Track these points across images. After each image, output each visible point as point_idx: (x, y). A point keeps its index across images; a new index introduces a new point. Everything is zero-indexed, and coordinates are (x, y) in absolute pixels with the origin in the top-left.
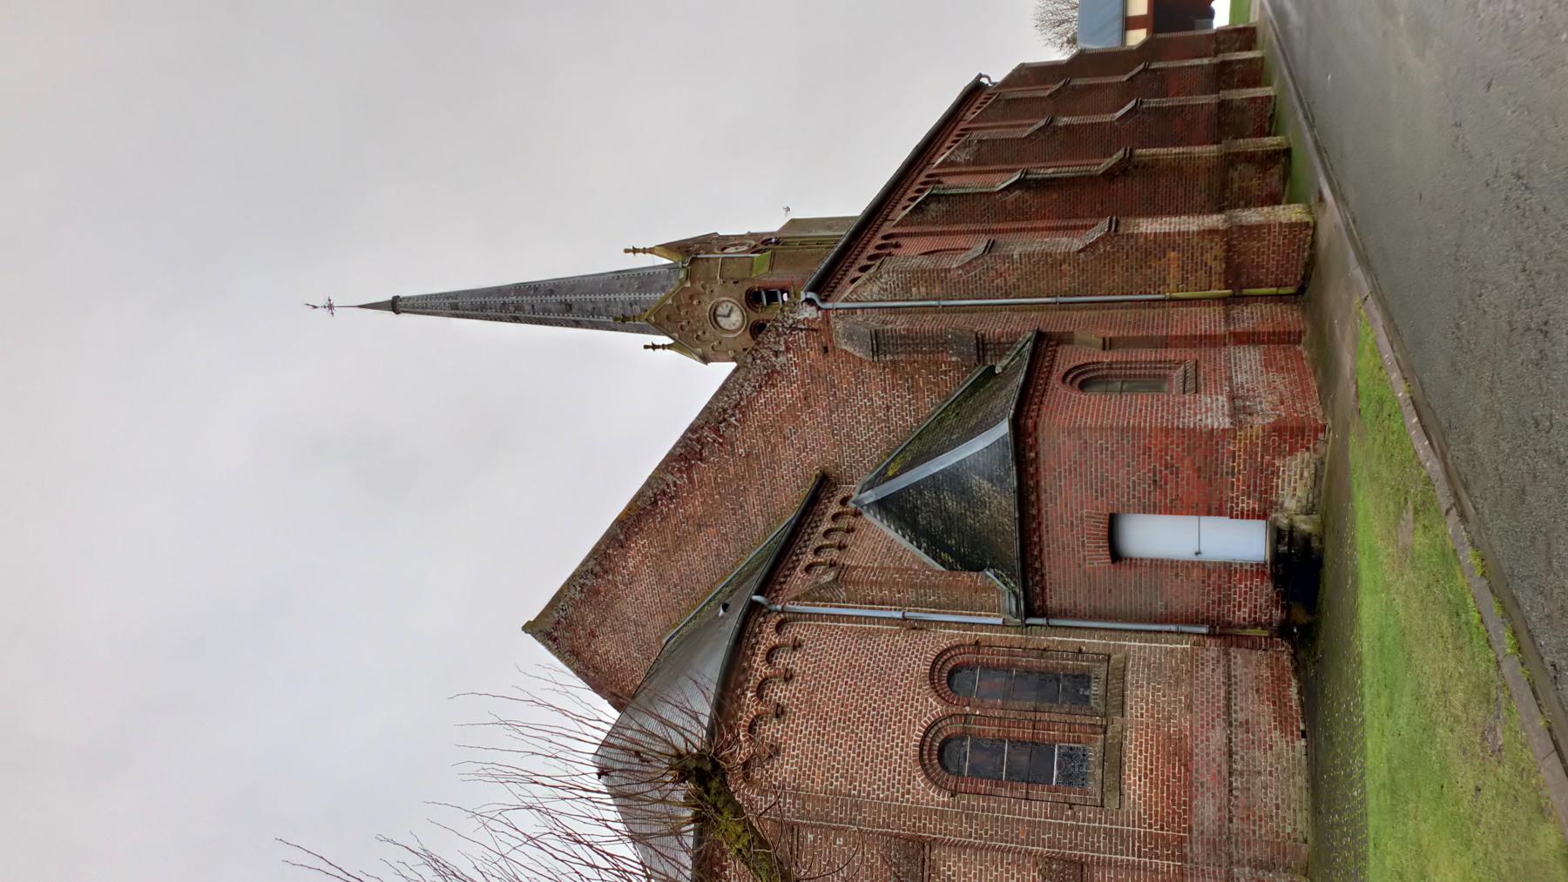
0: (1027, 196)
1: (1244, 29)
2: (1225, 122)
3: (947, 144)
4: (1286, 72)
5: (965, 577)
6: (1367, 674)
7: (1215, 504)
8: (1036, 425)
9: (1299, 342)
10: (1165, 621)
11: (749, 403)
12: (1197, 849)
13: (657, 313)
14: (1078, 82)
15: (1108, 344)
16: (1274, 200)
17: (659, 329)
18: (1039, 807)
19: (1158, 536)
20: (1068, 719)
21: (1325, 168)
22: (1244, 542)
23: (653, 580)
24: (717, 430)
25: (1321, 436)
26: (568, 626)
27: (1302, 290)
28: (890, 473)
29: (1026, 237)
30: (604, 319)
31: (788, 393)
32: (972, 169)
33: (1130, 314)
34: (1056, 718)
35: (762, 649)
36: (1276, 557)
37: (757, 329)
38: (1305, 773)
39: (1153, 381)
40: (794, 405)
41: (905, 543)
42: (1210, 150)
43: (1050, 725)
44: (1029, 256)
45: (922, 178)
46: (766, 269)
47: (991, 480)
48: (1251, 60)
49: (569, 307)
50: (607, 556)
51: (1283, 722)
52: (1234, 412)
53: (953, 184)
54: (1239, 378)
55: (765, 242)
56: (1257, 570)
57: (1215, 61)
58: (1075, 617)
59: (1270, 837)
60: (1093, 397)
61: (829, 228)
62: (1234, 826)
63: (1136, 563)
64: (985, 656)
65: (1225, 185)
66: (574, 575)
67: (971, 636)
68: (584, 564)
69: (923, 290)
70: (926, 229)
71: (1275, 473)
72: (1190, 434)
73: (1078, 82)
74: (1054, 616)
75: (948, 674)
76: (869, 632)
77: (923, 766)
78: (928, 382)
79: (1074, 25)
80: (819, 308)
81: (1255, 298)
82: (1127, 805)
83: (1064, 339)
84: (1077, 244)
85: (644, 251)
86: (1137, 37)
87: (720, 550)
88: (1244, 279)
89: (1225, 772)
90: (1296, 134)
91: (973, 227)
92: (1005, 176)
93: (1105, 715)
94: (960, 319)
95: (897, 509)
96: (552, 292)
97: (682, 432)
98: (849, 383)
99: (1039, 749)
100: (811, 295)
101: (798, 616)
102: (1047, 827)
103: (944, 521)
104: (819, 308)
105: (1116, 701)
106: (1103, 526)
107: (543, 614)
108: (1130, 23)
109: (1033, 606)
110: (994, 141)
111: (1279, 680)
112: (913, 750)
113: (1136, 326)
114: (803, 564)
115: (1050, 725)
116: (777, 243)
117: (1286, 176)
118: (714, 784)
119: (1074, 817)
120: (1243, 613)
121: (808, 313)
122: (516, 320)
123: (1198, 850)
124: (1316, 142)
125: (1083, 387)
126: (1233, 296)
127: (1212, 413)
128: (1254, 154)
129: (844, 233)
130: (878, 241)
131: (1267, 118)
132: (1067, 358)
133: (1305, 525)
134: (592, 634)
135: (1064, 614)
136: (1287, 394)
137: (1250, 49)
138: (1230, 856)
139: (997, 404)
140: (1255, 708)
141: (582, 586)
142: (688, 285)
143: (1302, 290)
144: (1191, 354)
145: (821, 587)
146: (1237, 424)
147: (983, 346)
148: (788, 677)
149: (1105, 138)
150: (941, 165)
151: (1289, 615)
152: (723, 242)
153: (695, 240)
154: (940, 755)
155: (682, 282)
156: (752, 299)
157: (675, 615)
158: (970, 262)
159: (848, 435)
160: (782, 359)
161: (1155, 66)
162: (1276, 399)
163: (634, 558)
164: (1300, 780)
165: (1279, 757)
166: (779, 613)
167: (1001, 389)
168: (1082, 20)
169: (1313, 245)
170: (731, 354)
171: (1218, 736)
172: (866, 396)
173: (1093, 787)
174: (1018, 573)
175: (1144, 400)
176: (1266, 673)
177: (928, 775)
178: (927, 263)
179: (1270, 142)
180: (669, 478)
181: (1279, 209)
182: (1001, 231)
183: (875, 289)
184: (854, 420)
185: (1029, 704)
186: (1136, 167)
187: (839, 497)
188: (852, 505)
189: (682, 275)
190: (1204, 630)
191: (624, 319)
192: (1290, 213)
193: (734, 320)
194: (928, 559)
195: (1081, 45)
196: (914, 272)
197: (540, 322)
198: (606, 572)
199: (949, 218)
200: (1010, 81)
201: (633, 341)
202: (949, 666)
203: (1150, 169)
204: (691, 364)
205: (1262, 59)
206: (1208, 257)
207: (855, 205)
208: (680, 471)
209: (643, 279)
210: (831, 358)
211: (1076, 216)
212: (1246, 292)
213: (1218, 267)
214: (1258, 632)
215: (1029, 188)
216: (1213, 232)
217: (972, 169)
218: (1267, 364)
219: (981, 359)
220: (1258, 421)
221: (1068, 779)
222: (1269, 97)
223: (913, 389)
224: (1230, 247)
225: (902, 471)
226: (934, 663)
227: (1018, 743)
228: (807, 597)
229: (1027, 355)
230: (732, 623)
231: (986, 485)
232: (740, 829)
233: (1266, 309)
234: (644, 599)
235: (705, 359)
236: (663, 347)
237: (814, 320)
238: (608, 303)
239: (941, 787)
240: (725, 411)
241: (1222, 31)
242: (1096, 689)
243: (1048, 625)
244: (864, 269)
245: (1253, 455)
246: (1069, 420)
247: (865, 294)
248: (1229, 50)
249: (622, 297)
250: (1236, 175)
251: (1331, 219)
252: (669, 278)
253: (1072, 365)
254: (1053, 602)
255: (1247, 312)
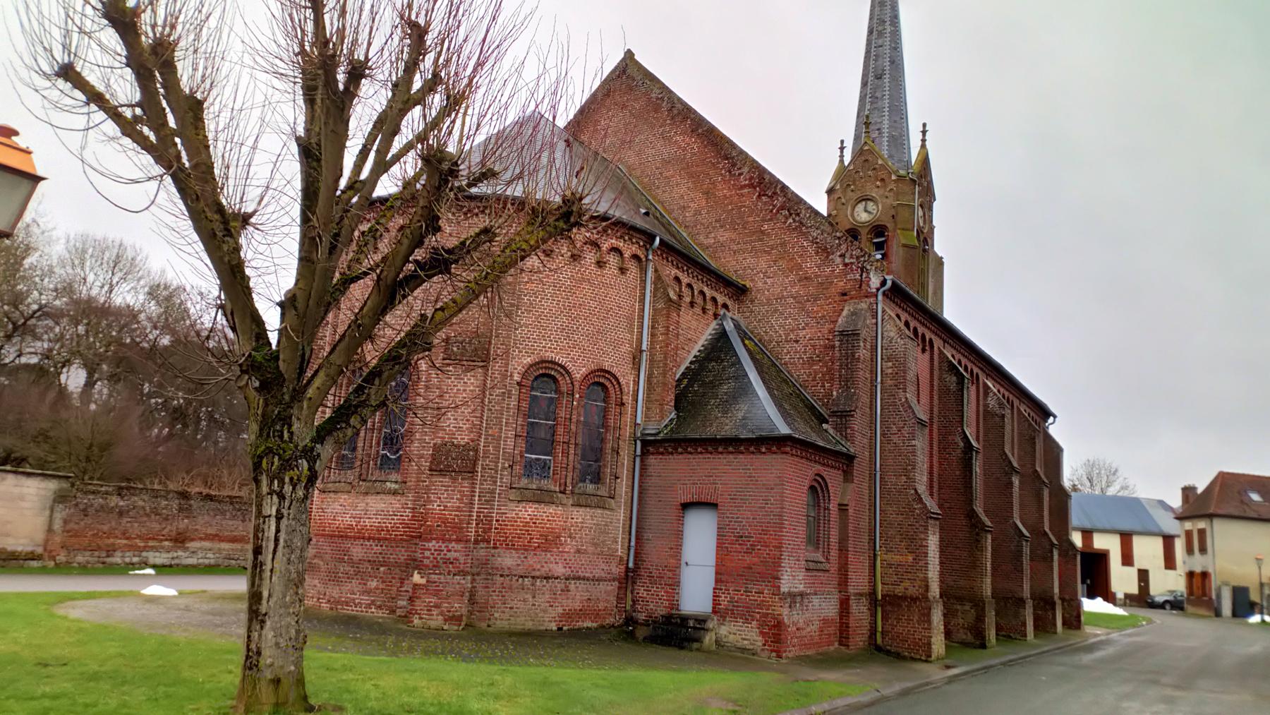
0: (959, 451)
1: (1079, 621)
2: (1008, 602)
3: (1002, 390)
4: (1046, 649)
5: (593, 367)
6: (615, 673)
7: (724, 578)
8: (786, 453)
9: (840, 644)
10: (637, 538)
11: (804, 234)
12: (483, 552)
13: (870, 152)
14: (1046, 493)
15: (843, 508)
16: (948, 634)
17: (859, 153)
18: (510, 441)
19: (700, 539)
20: (571, 467)
21: (973, 671)
22: (696, 595)
23: (666, 156)
24: (782, 208)
25: (774, 654)
26: (631, 88)
27: (879, 649)
28: (747, 342)
29: (927, 449)
30: (868, 107)
31: (811, 265)
32: (981, 409)
33: (865, 524)
34: (571, 457)
35: (621, 244)
36: (685, 619)
37: (853, 233)
38: (533, 628)
39: (814, 540)
40: (801, 268)
41: (695, 352)
42: (988, 591)
43: (566, 454)
44: (914, 453)
45: (976, 370)
46: (903, 242)
47: (744, 418)
48: (1055, 625)
49: (879, 77)
50: (685, 118)
51: (568, 615)
52: (792, 595)
53: (970, 394)
54: (816, 601)
55: (925, 241)
56: (674, 605)
57: (1056, 598)
58: (641, 475)
59: (491, 602)
60: (804, 497)
61: (935, 293)
62: (498, 578)
63: (680, 520)
64: (613, 410)
65: (960, 599)
66: (671, 92)
67: (628, 399)
68: (679, 99)
69: (890, 371)
70: (936, 373)
71: (746, 621)
72: (777, 564)
73: (1046, 493)
74: (642, 461)
75: (601, 383)
76: (632, 325)
77: (538, 363)
78: (816, 373)
79: (1087, 490)
80: (878, 290)
81: (874, 615)
82: (512, 505)
83: (848, 475)
84: (922, 489)
85: (924, 141)
86: (1077, 539)
87: (685, 205)
88: (889, 608)
89: (534, 574)
90: (997, 653)
91: (936, 410)
92: (974, 434)
93: (572, 492)
94: (865, 399)
95: (720, 346)
96: (892, 62)
97: (781, 179)
98: (817, 312)
99: (549, 446)
100: (889, 283)
101: (643, 271)
102: (497, 448)
103: (711, 382)
104: (878, 290)
105: (583, 500)
106: (709, 499)
107: (637, 63)
108: (1087, 534)
109: (650, 446)
110: (1003, 427)
111: (597, 615)
112: (549, 355)
113: (857, 529)
114: (680, 274)
115: (566, 454)
116: (925, 250)
117: (965, 645)
118: (561, 224)
119: (504, 468)
120: (642, 592)
121: (875, 281)
122: (870, 32)
123: (481, 552)
124: (991, 666)
125: (812, 488)
126: (876, 600)
127: (792, 580)
128: (983, 622)
129: (930, 305)
130: (928, 335)
131: (1010, 633)
132: (833, 477)
133: (708, 639)
134: (624, 107)
135: (644, 468)
136: (804, 633)
137: (1064, 624)
138: (478, 574)
139: (801, 425)
140: (578, 596)
141: (662, 99)
142: (894, 177)
143: (879, 649)
144: (833, 566)
145: (665, 289)
146: (784, 596)
147: (843, 416)
148: (600, 264)
149: (1001, 511)
150: (985, 385)
151: (642, 624)
152: (927, 206)
153: (930, 183)
154: (546, 375)
155: (896, 172)
156: (878, 230)
157: (638, 173)
158: (910, 407)
159: (776, 311)
160: (838, 260)
161: (1056, 553)
162: (801, 625)
163: (685, 141)
164: (529, 625)
165: (545, 611)
166: (646, 257)
167: (812, 428)
168: (1092, 497)
169: (913, 659)
170: (834, 213)
171: (559, 570)
172: (807, 325)
173: (524, 482)
174: (675, 436)
175: (802, 530)
176: (601, 605)
177: (531, 366)
178: (911, 375)
179: (991, 634)
180: (745, 170)
181: (942, 637)
182: (931, 431)
183: (892, 334)
184: (787, 310)
185: (580, 440)
186: (978, 534)
187: (729, 303)
188: (722, 312)
189: (902, 172)
190: (631, 565)
191: (867, 124)
192: (938, 644)
193: (862, 215)
194: (682, 369)
195: (1073, 494)
196: (904, 364)
197: (868, 52)
198: (672, 118)
199: (944, 391)
200: (1049, 440)
201: (847, 129)
202: (607, 383)
203: (976, 544)
204: (826, 182)
205: (1055, 633)
206: (907, 584)
207: (951, 313)
208: (751, 178)
209: (899, 140)
210: (837, 298)
211: (940, 488)
212: (879, 609)
213: (899, 590)
214: (630, 602)
215: (965, 453)
216: (927, 588)
217: (981, 409)
218: (825, 621)
219: (834, 414)
220: (785, 611)
221: (529, 465)
222: (1025, 636)
223: (811, 362)
224: (914, 599)
225: (748, 350)
226: (608, 372)
227: (553, 429)
228: (658, 278)
229: (839, 448)
230: (639, 222)
231: (740, 415)
232: (532, 243)
233: (866, 623)
234: (650, 152)
235: (830, 192)
236: (842, 156)
237: (868, 286)
238: (881, 110)
239: (524, 376)
240: (798, 215)
241: (1079, 606)
242: (590, 488)
243: (635, 456)
244: (907, 324)
245: (760, 606)
246: (787, 480)
247: (889, 326)
248: (1064, 609)
249: (886, 122)
250: (967, 608)
251: (935, 673)
252: (900, 161)
253: (827, 478)
254: (652, 460)
255: (865, 609)
